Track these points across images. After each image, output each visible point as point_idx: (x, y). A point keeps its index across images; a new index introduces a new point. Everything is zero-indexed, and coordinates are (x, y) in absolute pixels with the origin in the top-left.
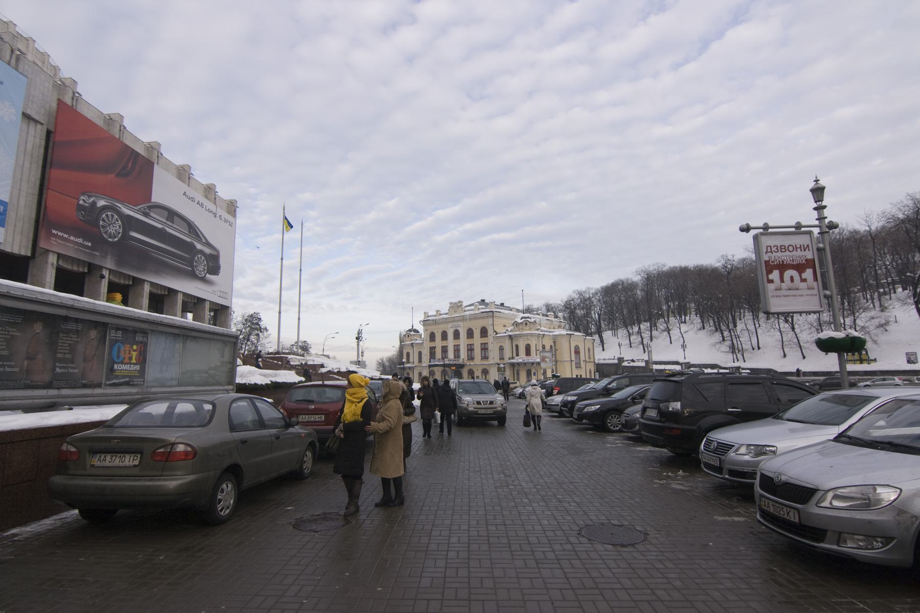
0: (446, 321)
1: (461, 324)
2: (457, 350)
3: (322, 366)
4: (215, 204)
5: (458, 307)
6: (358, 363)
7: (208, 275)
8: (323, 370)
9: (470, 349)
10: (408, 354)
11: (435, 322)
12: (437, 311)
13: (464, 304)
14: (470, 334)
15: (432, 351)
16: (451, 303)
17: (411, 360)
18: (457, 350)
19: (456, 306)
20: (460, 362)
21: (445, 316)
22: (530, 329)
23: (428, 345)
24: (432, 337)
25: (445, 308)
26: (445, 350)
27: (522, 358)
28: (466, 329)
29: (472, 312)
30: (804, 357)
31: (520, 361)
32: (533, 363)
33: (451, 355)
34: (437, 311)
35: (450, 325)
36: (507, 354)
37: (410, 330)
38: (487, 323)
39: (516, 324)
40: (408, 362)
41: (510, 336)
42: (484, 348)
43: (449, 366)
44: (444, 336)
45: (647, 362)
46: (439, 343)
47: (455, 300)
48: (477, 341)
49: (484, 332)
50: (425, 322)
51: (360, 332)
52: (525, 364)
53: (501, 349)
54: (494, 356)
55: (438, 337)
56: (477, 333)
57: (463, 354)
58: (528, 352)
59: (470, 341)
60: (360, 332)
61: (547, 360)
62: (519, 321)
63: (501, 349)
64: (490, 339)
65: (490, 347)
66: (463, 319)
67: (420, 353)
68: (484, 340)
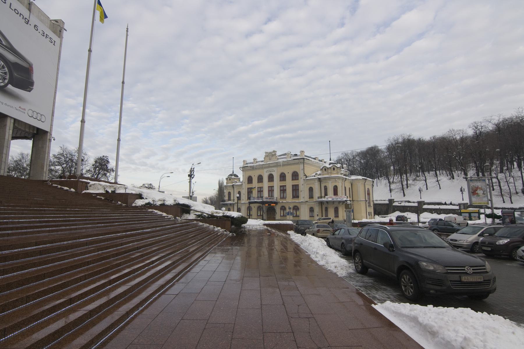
0: (262, 167)
1: (275, 169)
2: (271, 190)
3: (140, 196)
4: (30, 10)
5: (273, 155)
6: (191, 197)
7: (10, 86)
8: (139, 203)
9: (283, 190)
10: (229, 193)
11: (253, 168)
12: (255, 159)
13: (278, 153)
14: (283, 177)
15: (250, 191)
16: (266, 153)
17: (232, 198)
18: (271, 190)
19: (271, 155)
20: (275, 200)
21: (261, 163)
22: (338, 173)
23: (246, 186)
24: (250, 180)
25: (260, 157)
26: (260, 191)
27: (331, 197)
28: (279, 174)
29: (285, 160)
30: (504, 202)
31: (330, 199)
32: (340, 202)
33: (266, 194)
34: (255, 159)
35: (265, 170)
36: (316, 194)
37: (231, 175)
38: (298, 168)
39: (325, 169)
40: (229, 199)
41: (319, 179)
42: (296, 189)
43: (263, 203)
44: (260, 179)
45: (419, 203)
46: (255, 184)
47: (270, 150)
48: (289, 183)
49: (295, 176)
50: (244, 169)
51: (192, 171)
52: (333, 202)
53: (311, 190)
54: (304, 194)
55: (255, 180)
56: (289, 177)
57: (277, 194)
58: (336, 193)
59: (283, 183)
60: (192, 171)
61: (480, 192)
62: (328, 166)
63: (311, 190)
64: (301, 182)
65: (301, 188)
66: (277, 165)
67: (239, 193)
68: (295, 182)
